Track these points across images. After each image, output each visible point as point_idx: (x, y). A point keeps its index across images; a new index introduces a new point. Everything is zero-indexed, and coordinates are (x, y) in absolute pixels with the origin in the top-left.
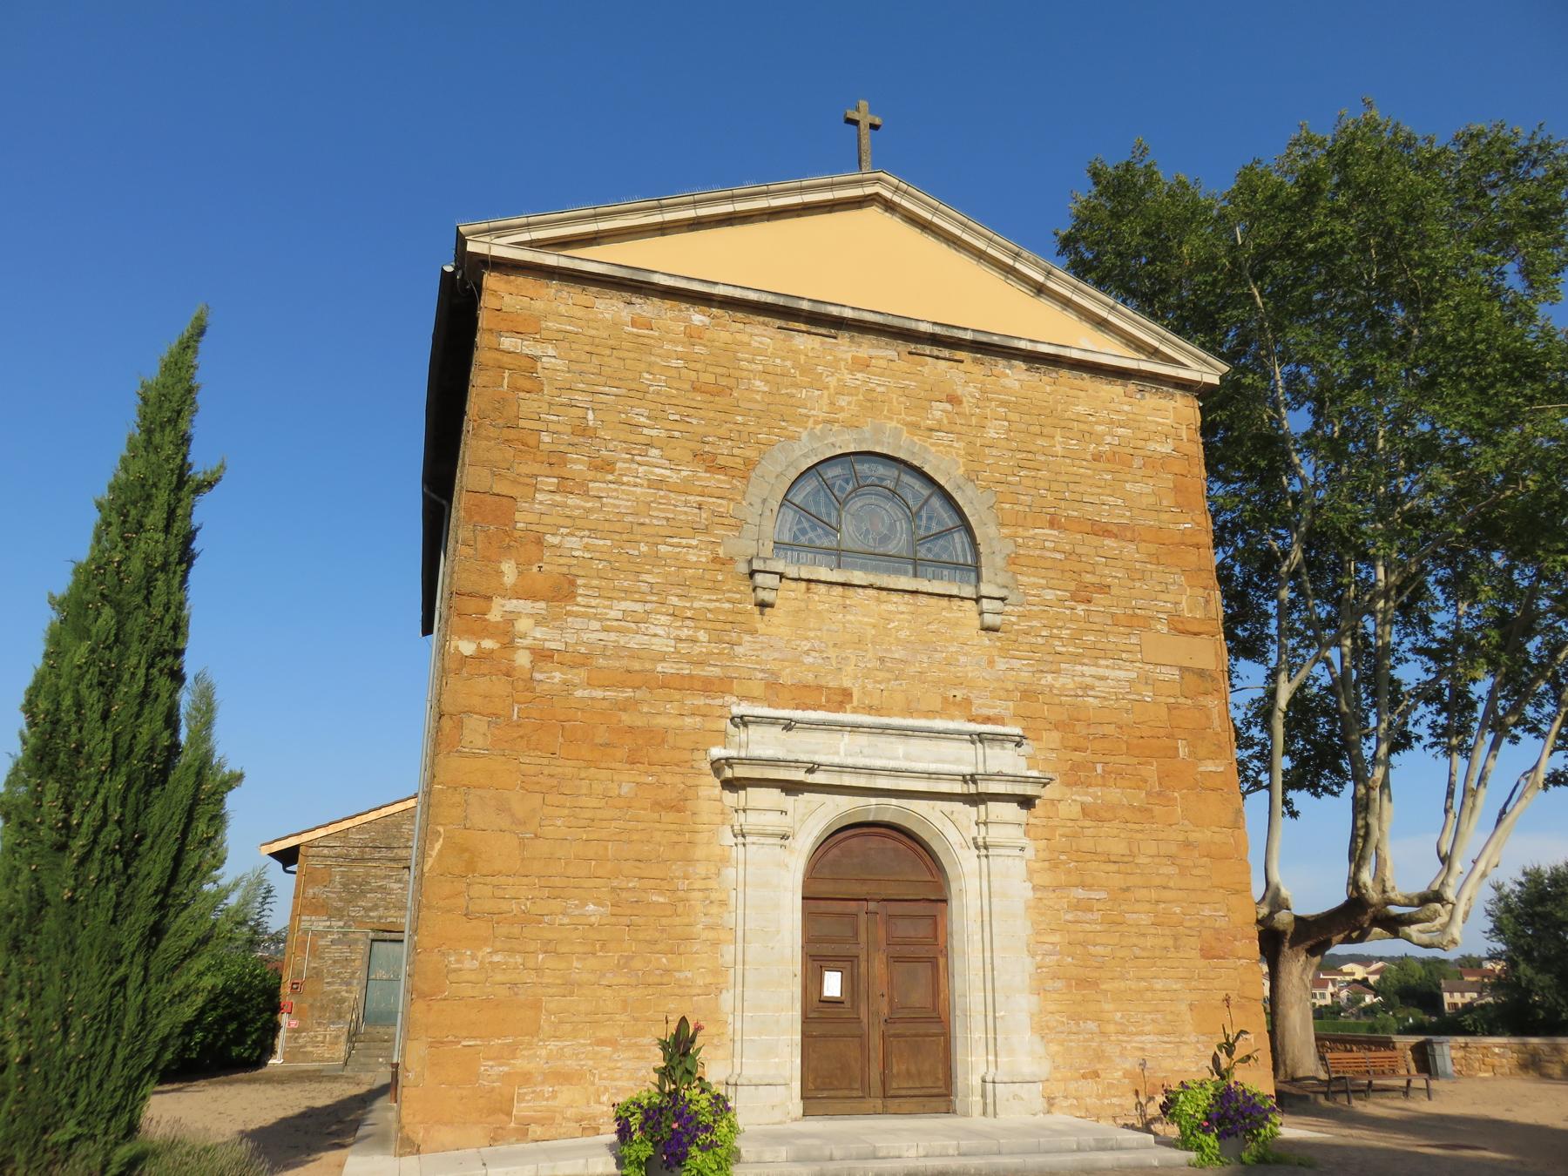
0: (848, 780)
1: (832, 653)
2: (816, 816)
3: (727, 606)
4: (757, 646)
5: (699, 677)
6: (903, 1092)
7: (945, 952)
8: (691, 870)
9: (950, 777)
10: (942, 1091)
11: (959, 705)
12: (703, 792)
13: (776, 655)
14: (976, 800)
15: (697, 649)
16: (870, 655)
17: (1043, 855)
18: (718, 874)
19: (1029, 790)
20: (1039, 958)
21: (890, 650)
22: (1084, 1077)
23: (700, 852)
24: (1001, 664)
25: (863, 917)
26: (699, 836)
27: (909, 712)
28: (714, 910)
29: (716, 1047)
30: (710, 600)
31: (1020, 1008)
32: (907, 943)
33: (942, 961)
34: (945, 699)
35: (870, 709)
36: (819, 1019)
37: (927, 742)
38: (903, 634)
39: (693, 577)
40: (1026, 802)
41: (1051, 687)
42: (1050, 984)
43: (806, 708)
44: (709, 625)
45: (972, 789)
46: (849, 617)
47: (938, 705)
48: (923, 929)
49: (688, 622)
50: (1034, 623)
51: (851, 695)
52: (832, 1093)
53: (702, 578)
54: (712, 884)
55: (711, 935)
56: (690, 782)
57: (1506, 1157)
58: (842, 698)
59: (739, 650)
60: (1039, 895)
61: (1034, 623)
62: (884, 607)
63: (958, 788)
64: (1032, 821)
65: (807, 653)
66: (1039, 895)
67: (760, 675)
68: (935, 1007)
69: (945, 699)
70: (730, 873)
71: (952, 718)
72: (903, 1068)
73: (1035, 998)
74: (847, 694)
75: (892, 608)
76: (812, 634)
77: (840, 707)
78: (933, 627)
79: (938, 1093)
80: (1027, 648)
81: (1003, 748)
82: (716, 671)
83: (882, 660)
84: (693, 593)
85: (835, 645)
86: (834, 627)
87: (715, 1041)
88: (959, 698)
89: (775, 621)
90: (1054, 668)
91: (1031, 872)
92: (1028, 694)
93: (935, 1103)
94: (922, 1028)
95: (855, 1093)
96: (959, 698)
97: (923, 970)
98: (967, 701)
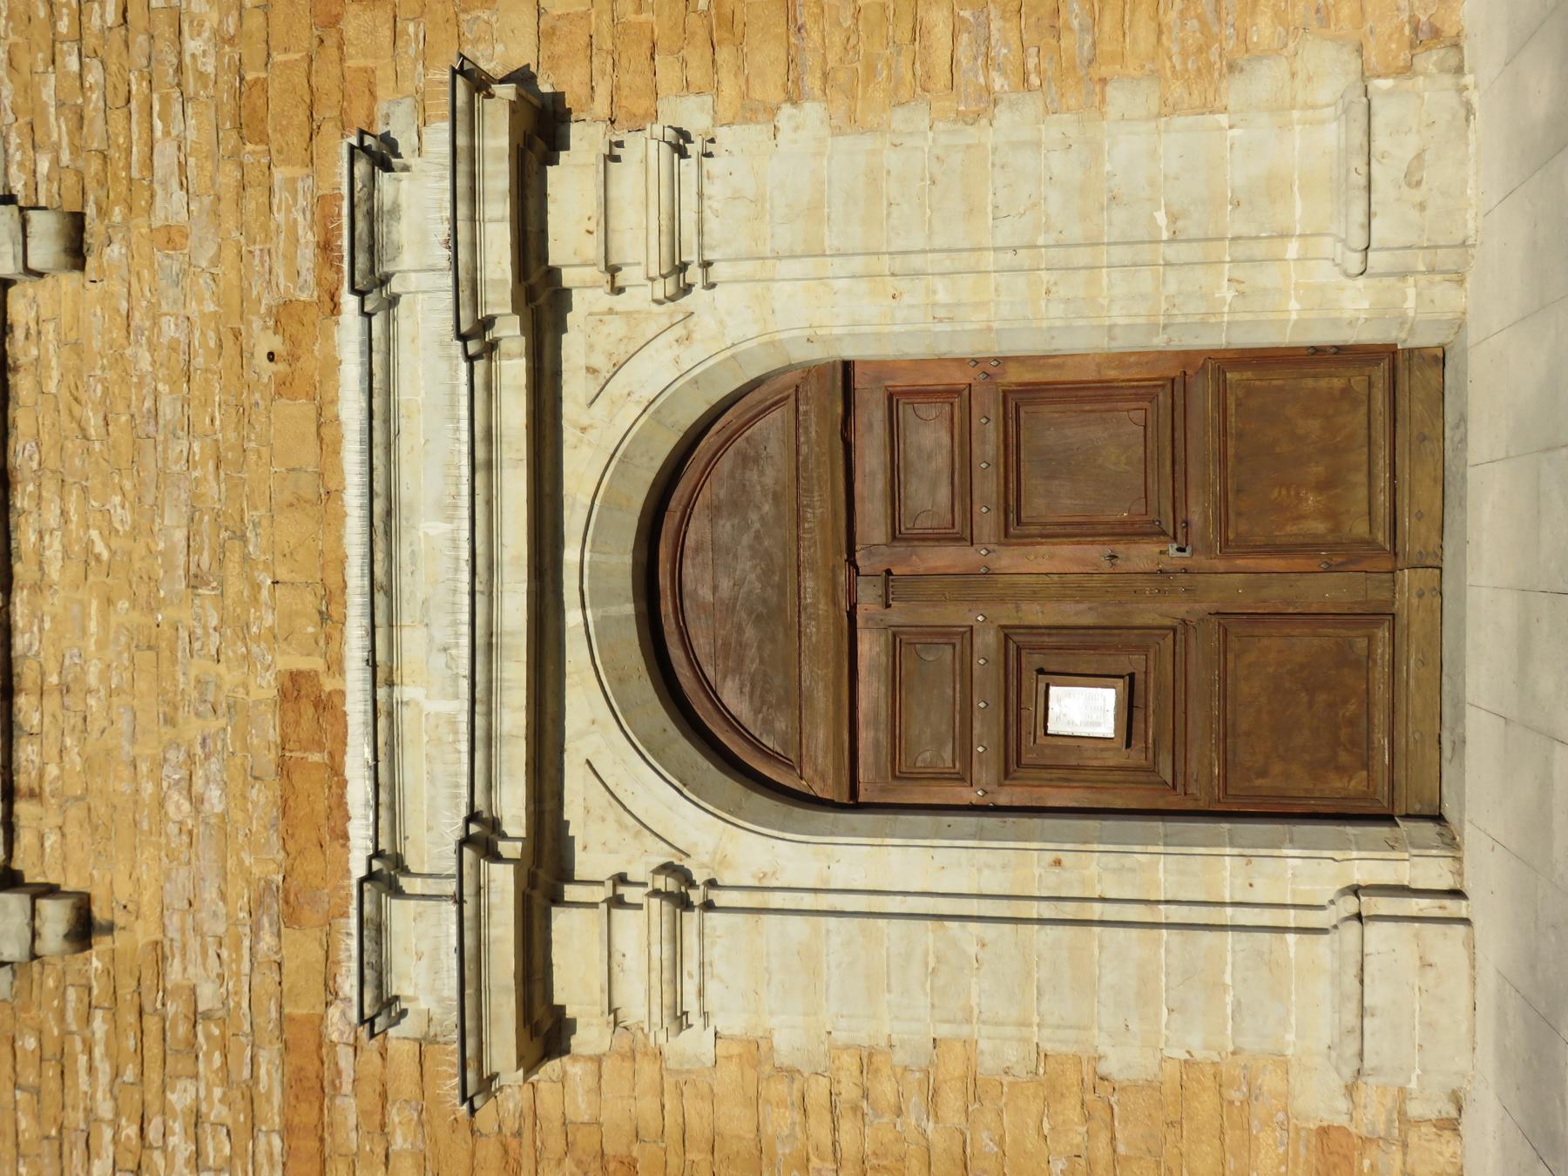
0: (513, 717)
1: (192, 729)
2: (630, 800)
3: (99, 1025)
4: (194, 944)
5: (287, 1109)
6: (1382, 499)
7: (989, 367)
8: (782, 1150)
9: (482, 394)
10: (1380, 373)
11: (293, 341)
12: (581, 1107)
13: (210, 893)
14: (542, 298)
15: (217, 1111)
16: (186, 616)
17: (697, 55)
18: (791, 1073)
19: (496, 139)
20: (998, 82)
21: (167, 554)
23: (736, 1121)
24: (171, 206)
25: (899, 614)
26: (694, 1123)
28: (885, 1089)
29: (1253, 1095)
30: (91, 1069)
31: (1139, 143)
32: (963, 490)
33: (1015, 376)
34: (283, 387)
35: (329, 618)
36: (1181, 778)
37: (404, 445)
38: (122, 516)
39: (38, 1118)
40: (543, 129)
41: (223, 40)
42: (1074, 44)
43: (339, 807)
44: (153, 1075)
45: (510, 331)
46: (92, 680)
47: (298, 411)
48: (929, 437)
49: (153, 1134)
50: (48, 94)
51: (295, 677)
52: (1380, 718)
53: (37, 1092)
54: (818, 1091)
55: (952, 1102)
56: (555, 1144)
57: (1297, 196)
58: (306, 698)
59: (208, 997)
60: (812, 82)
61: (48, 94)
62: (54, 571)
63: (513, 370)
64: (601, 106)
65: (197, 802)
66: (812, 82)
67: (267, 940)
68: (1141, 392)
69: (283, 387)
70: (788, 1041)
71: (332, 365)
72: (1311, 500)
73: (1118, 98)
74: (295, 688)
75: (54, 546)
76: (148, 788)
77: (329, 706)
78: (94, 423)
79: (1381, 396)
80: (117, 117)
81: (395, 211)
82: (268, 1058)
83: (195, 581)
84: (76, 1118)
85: (170, 721)
86: (124, 724)
87: (1236, 1096)
88: (276, 343)
89: (123, 891)
90: (165, 31)
91: (751, 111)
92: (246, 119)
93: (1414, 406)
94: (1201, 441)
95: (1382, 651)
96: (276, 343)
97: (1053, 431)
98: (284, 315)
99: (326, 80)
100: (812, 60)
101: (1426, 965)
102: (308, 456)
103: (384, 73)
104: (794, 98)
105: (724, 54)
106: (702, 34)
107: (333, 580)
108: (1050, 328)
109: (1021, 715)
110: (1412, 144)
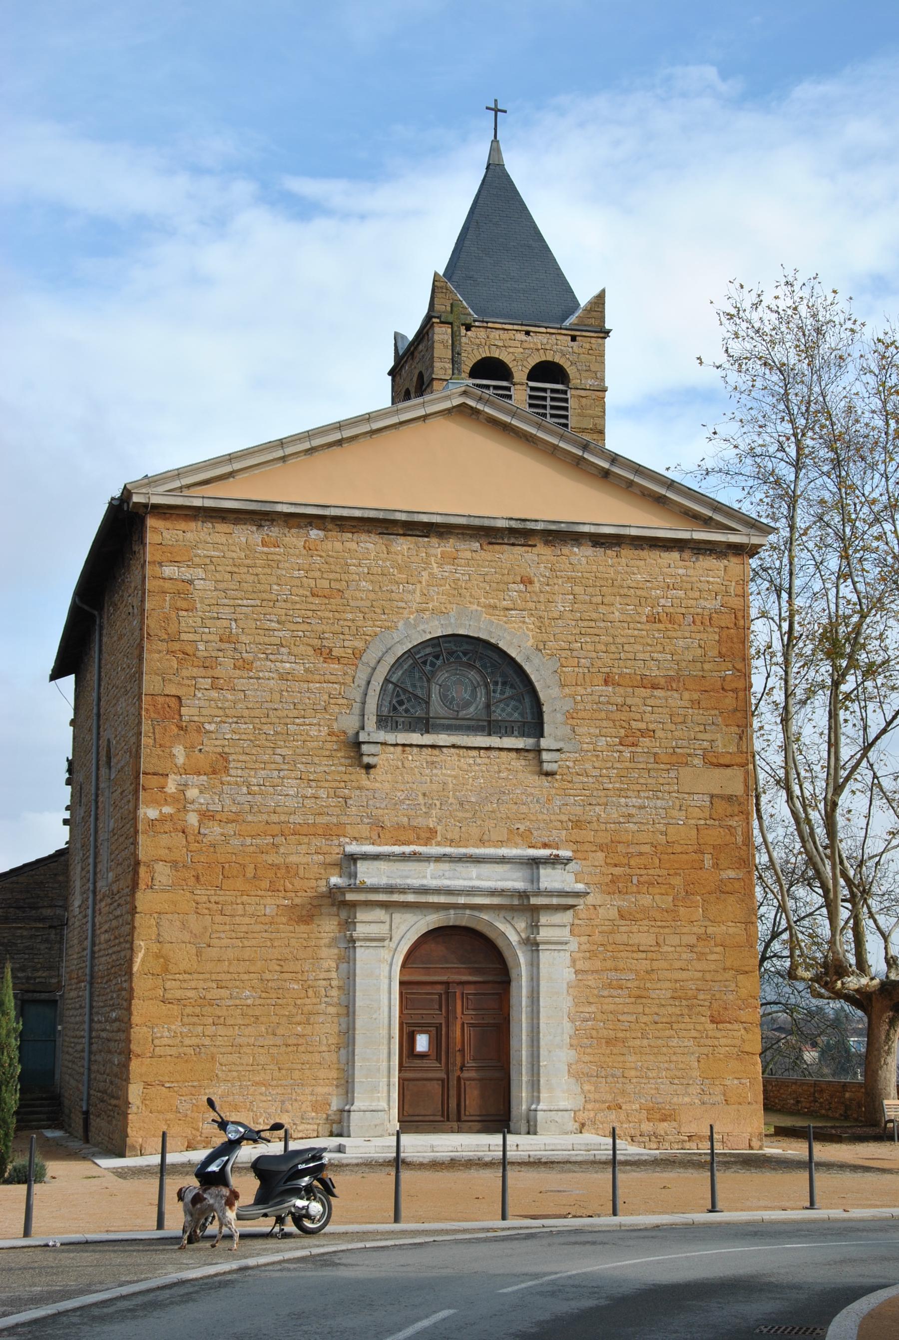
22: (609, 1108)
27: (482, 842)
35: (451, 842)
58: (429, 836)
66: (580, 977)
69: (510, 831)
73: (573, 1052)
74: (433, 832)
81: (554, 869)
88: (522, 830)
96: (522, 830)
99: (586, 847)
100: (585, 977)
101: (376, 1126)
102: (494, 837)
103: (588, 863)
104: (576, 972)
105: (588, 954)
106: (592, 948)
107: (461, 844)
108: (815, 1084)
109: (423, 1028)
110: (559, 1120)
